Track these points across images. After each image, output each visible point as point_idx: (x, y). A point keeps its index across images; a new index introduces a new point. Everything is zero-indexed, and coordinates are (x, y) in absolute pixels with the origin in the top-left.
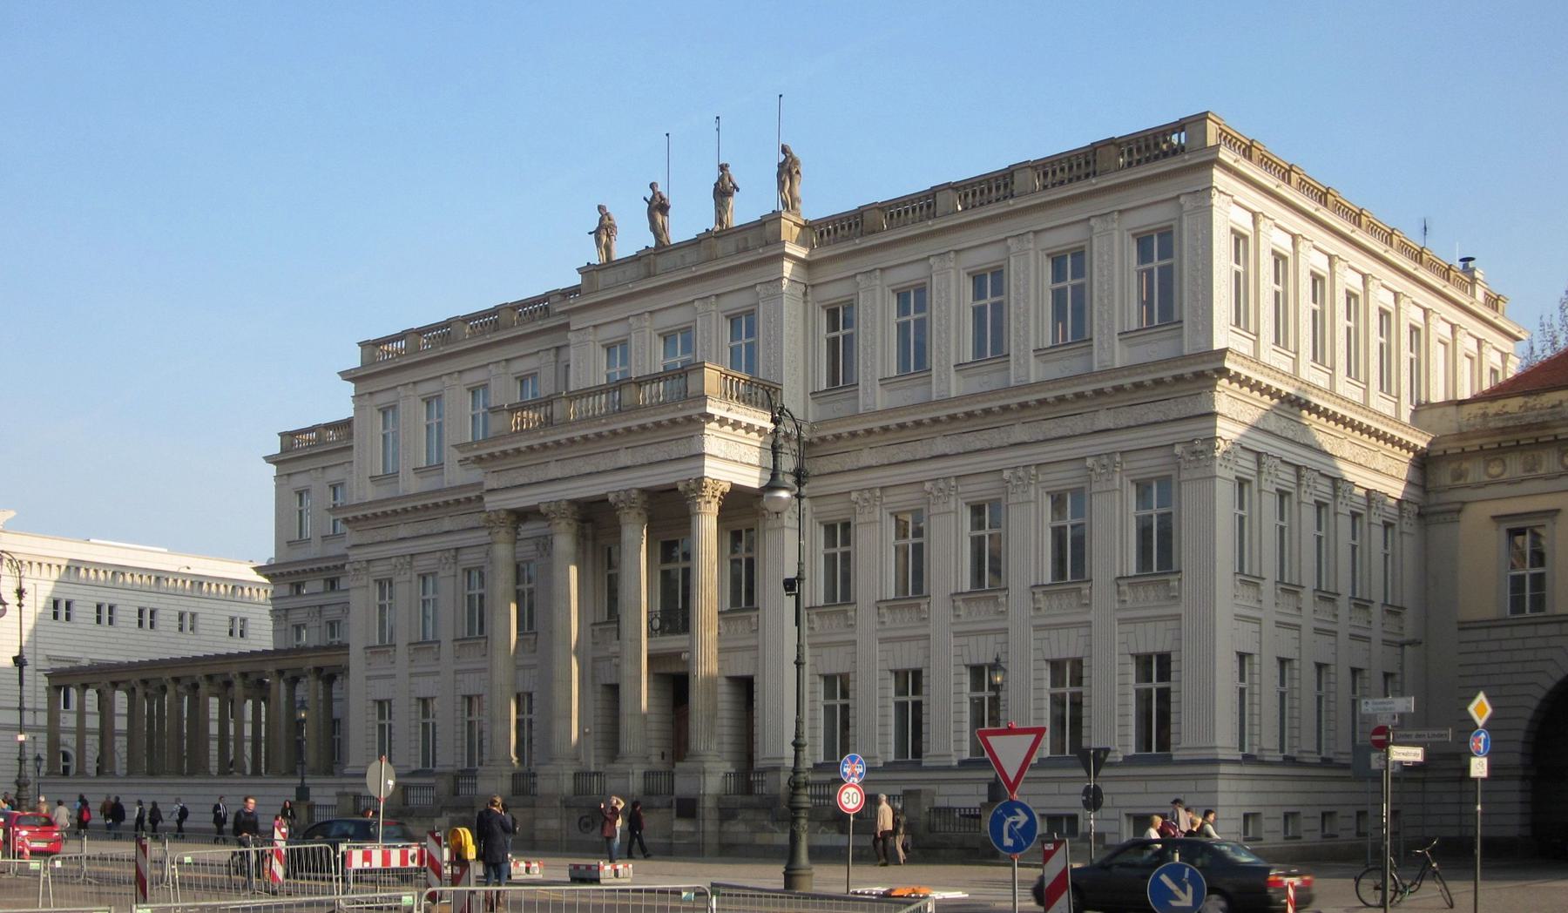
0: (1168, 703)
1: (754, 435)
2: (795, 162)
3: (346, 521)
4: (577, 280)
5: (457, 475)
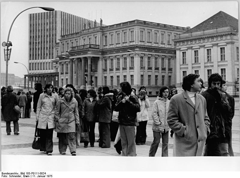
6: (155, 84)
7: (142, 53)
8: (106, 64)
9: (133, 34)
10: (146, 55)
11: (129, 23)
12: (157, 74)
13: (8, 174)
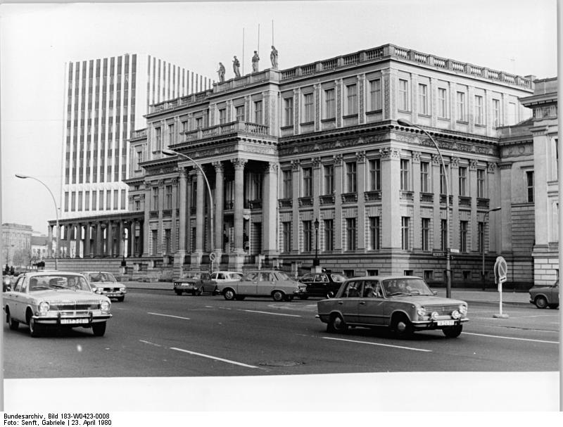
0: (529, 197)
1: (273, 145)
2: (277, 51)
3: (144, 167)
6: (420, 246)
7: (481, 159)
9: (259, 109)
10: (415, 154)
11: (365, 57)
12: (426, 214)
13: (20, 417)
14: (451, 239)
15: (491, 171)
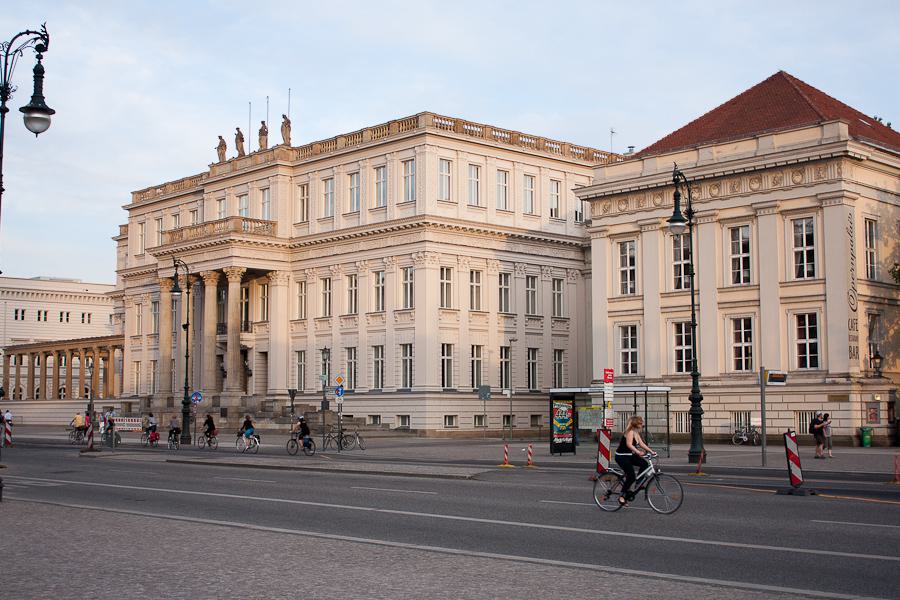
2: (289, 122)
4: (208, 169)
5: (150, 260)
6: (525, 385)
8: (303, 300)
14: (565, 370)
15: (572, 281)
